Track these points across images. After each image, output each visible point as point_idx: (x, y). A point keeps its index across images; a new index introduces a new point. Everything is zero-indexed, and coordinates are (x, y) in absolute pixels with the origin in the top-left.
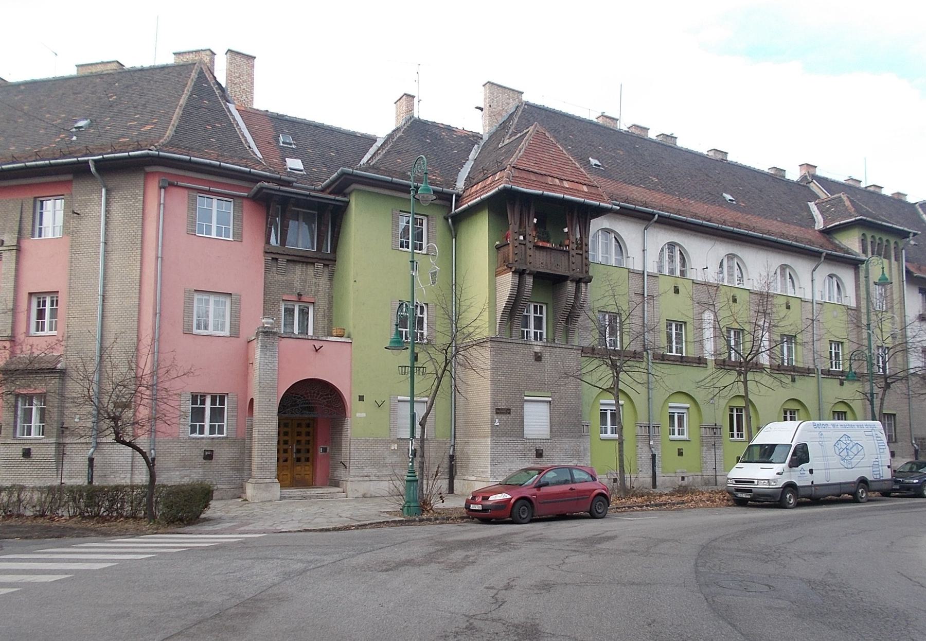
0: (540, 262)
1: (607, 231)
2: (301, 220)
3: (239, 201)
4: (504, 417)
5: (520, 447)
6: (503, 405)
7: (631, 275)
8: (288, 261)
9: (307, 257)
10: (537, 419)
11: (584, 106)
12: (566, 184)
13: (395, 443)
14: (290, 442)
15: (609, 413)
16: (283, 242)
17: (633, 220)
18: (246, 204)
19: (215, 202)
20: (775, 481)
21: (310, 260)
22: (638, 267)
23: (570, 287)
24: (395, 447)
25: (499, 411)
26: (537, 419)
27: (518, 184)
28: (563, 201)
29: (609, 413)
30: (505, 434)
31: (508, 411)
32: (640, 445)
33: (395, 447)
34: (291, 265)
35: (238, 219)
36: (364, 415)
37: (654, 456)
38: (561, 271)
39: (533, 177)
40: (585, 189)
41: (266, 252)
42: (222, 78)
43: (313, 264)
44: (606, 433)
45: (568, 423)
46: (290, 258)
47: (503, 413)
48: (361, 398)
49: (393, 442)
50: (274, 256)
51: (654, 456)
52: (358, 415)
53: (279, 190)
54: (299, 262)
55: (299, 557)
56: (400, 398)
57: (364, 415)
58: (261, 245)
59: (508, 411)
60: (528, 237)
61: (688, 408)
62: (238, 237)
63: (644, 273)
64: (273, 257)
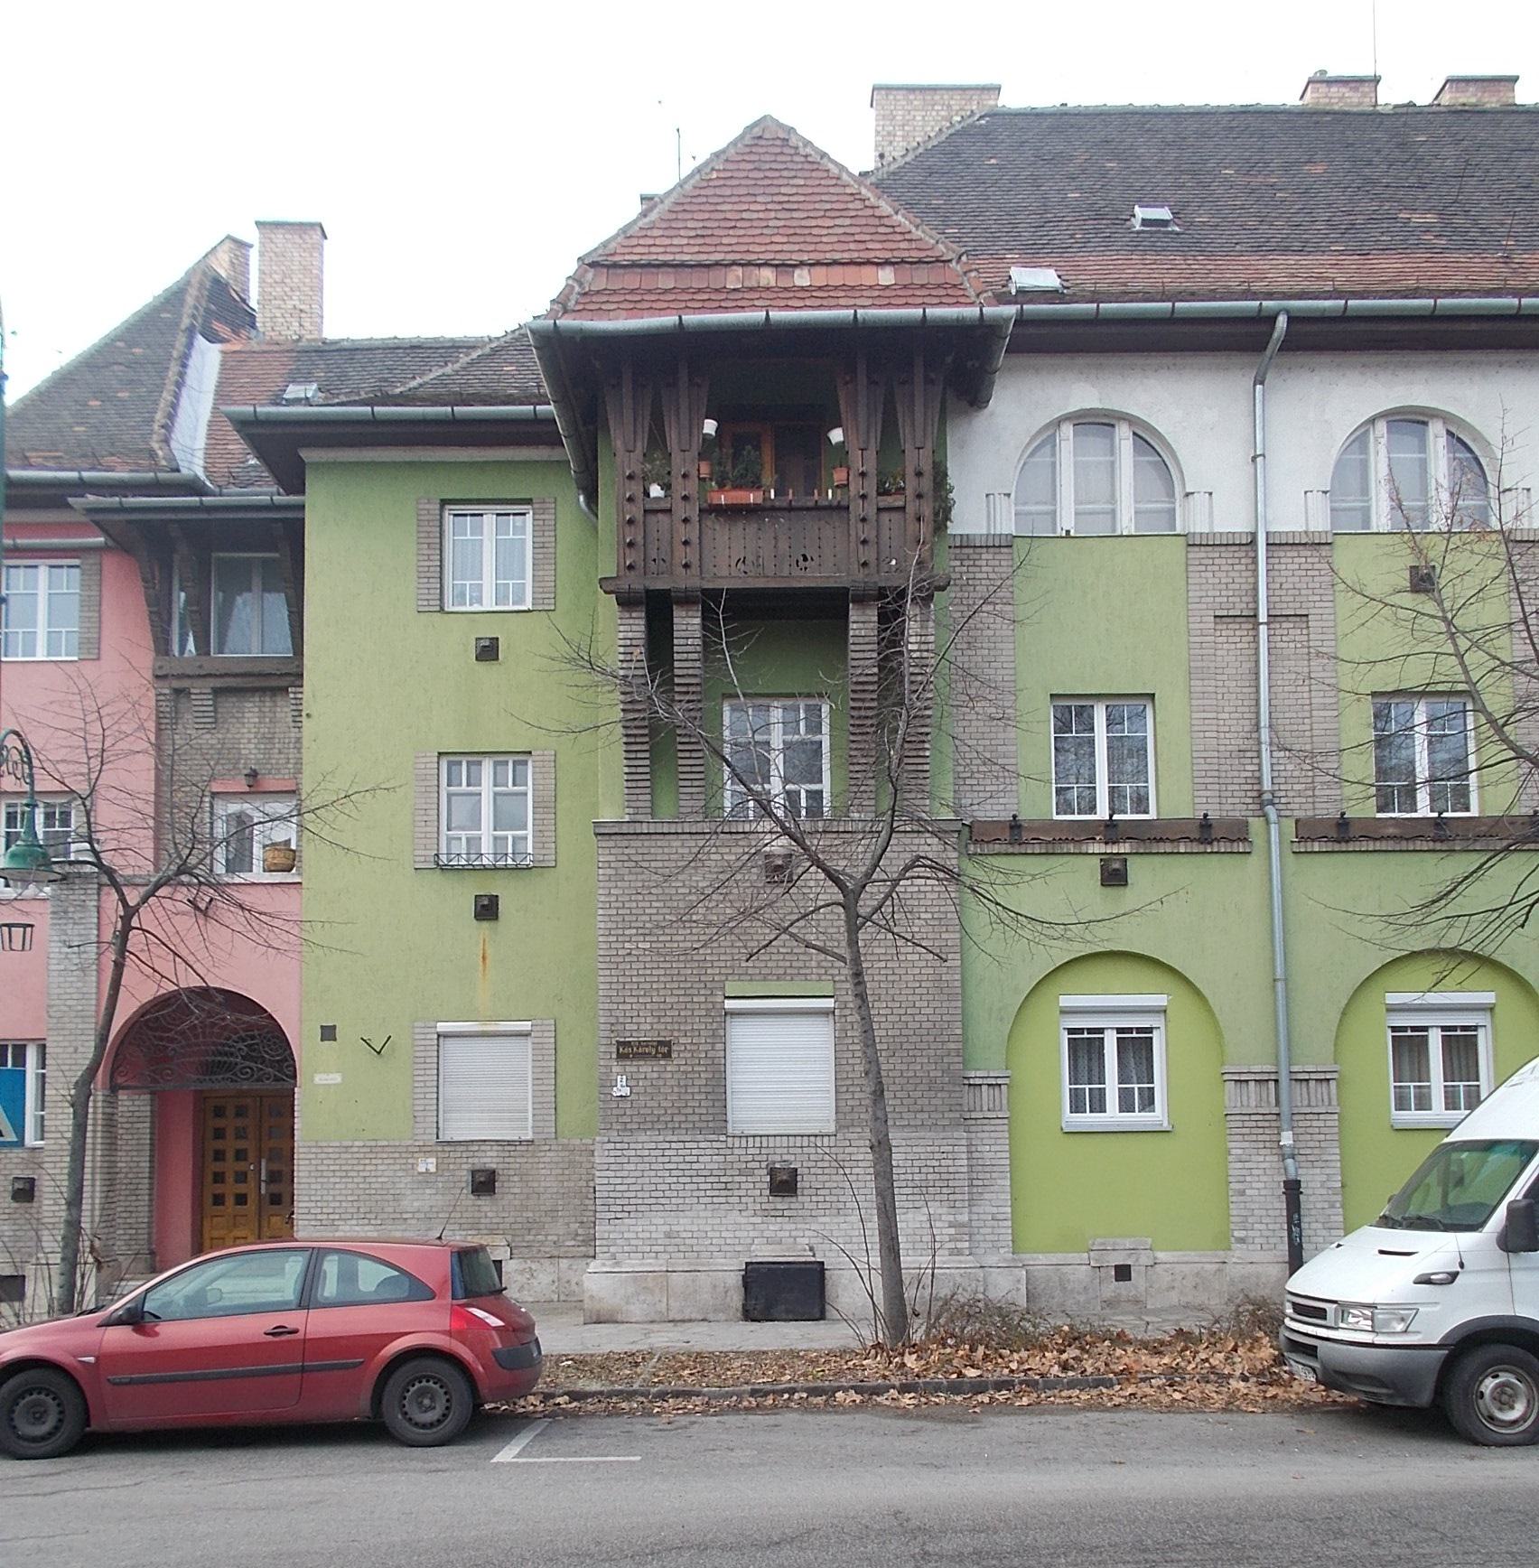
0: (736, 558)
1: (1098, 422)
2: (257, 582)
3: (93, 559)
4: (646, 1068)
5: (709, 1162)
6: (644, 1030)
7: (1197, 554)
8: (217, 692)
9: (260, 675)
10: (783, 1070)
11: (1263, 72)
12: (802, 278)
13: (428, 1153)
14: (251, 1155)
15: (1435, 1041)
16: (203, 647)
17: (1206, 359)
18: (111, 564)
19: (43, 573)
20: (1405, 1312)
21: (274, 683)
22: (1230, 520)
23: (863, 624)
24: (430, 1164)
25: (627, 1051)
26: (783, 1070)
27: (599, 312)
28: (768, 334)
29: (1435, 1041)
30: (650, 1122)
31: (663, 1050)
32: (1237, 1148)
33: (430, 1164)
34: (228, 704)
35: (92, 605)
36: (337, 1078)
37: (1293, 1190)
38: (818, 575)
39: (666, 281)
40: (886, 276)
41: (157, 677)
42: (253, 304)
43: (285, 690)
44: (1099, 1105)
45: (907, 1085)
46: (219, 683)
47: (644, 1056)
48: (328, 1033)
49: (425, 1151)
50: (176, 684)
51: (1293, 1190)
52: (318, 1079)
53: (122, 509)
54: (254, 690)
55: (1466, 1377)
56: (443, 1027)
57: (337, 1078)
58: (146, 659)
59: (663, 1050)
60: (677, 483)
61: (1490, 1009)
62: (92, 648)
63: (1253, 542)
64: (175, 688)
